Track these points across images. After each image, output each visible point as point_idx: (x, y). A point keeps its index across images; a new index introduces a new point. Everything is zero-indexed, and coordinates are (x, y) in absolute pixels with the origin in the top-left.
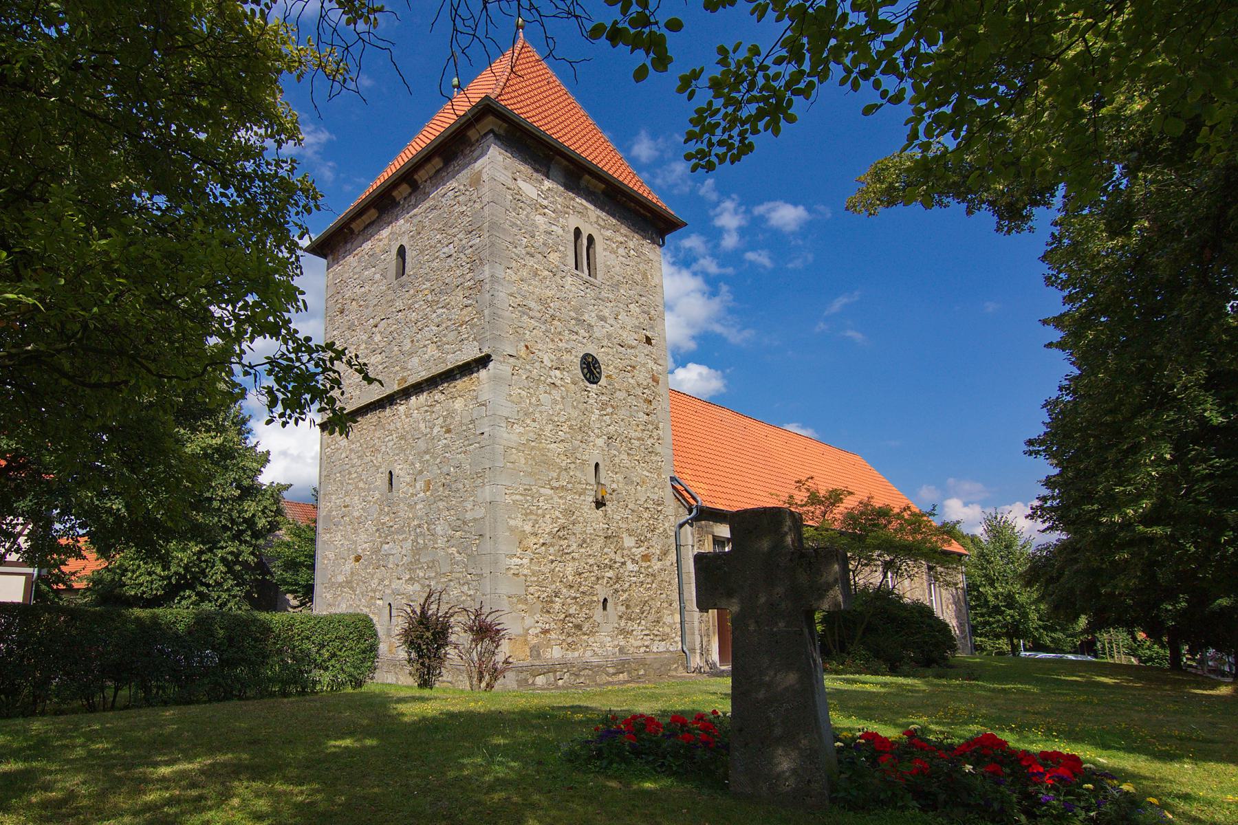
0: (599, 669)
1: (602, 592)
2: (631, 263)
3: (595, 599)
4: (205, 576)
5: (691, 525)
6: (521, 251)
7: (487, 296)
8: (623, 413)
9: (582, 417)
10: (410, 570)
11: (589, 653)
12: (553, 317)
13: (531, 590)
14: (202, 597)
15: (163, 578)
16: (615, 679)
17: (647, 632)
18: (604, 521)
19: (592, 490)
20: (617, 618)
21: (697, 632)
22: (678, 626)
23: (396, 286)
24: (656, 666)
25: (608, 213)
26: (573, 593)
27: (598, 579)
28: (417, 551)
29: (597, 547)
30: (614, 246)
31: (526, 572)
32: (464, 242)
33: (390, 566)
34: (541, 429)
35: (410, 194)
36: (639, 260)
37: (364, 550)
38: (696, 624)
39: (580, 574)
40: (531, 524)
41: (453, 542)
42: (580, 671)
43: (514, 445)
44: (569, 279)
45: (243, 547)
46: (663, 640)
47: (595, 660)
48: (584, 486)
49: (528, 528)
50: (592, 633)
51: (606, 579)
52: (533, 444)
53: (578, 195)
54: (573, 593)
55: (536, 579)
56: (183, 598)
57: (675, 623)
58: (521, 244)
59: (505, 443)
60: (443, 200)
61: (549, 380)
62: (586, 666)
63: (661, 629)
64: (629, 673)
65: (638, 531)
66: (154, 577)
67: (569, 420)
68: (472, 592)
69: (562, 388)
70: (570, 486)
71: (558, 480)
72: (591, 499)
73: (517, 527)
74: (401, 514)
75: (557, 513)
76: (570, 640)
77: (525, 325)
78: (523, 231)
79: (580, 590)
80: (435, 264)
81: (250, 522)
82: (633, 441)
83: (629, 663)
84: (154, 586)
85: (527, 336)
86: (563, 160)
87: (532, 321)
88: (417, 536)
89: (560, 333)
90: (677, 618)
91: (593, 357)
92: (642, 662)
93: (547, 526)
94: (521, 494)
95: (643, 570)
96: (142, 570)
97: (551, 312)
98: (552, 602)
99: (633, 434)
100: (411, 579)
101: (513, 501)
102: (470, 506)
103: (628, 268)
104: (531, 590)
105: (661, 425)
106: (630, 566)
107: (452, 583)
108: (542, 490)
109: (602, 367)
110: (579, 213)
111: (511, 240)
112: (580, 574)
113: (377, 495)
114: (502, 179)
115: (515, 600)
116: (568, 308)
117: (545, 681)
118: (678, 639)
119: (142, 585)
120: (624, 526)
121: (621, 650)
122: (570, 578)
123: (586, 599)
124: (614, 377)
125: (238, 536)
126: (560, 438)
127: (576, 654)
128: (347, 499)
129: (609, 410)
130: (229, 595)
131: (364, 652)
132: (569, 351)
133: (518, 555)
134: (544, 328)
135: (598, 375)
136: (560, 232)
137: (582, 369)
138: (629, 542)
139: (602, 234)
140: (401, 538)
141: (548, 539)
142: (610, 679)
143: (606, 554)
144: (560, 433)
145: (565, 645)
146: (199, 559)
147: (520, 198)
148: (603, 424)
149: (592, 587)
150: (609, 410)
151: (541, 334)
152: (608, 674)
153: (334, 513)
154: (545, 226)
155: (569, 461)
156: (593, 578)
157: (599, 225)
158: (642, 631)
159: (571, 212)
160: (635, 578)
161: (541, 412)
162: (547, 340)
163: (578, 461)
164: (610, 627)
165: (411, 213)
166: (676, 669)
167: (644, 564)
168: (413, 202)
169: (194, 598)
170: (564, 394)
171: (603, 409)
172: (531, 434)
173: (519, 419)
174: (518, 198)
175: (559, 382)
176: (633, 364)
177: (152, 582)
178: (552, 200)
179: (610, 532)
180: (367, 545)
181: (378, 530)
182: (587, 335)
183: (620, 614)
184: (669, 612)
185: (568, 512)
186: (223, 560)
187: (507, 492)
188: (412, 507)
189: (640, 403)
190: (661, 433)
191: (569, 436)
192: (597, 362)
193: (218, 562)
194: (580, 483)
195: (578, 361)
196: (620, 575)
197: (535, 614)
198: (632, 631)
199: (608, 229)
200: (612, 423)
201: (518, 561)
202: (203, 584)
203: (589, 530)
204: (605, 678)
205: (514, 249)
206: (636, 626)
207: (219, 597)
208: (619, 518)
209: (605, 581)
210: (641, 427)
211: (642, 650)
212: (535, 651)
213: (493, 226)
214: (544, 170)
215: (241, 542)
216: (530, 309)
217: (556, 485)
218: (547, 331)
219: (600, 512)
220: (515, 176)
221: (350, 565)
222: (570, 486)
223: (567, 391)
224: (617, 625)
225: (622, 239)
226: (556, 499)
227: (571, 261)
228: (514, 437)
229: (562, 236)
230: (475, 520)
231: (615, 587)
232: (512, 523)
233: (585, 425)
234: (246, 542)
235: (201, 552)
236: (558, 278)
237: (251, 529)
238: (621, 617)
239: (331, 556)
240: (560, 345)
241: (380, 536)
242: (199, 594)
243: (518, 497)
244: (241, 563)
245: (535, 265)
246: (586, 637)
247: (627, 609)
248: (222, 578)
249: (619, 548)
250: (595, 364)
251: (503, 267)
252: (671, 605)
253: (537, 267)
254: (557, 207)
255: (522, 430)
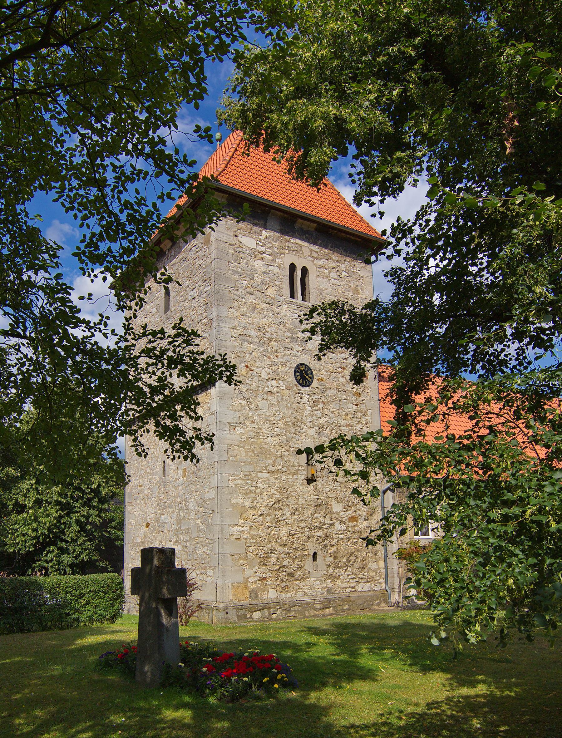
0: (309, 605)
1: (311, 548)
2: (343, 283)
3: (306, 553)
4: (65, 535)
5: (393, 491)
6: (242, 292)
7: (214, 331)
8: (333, 406)
9: (296, 415)
10: (176, 535)
11: (300, 594)
12: (270, 340)
13: (251, 549)
14: (63, 551)
15: (33, 538)
16: (322, 612)
17: (353, 576)
18: (315, 494)
19: (304, 470)
20: (325, 567)
21: (396, 575)
22: (383, 570)
23: (165, 319)
24: (360, 602)
25: (320, 246)
26: (286, 550)
27: (309, 538)
28: (180, 521)
29: (307, 513)
30: (326, 271)
31: (246, 536)
32: (201, 288)
33: (165, 531)
34: (259, 428)
35: (171, 247)
36: (350, 279)
37: (151, 519)
38: (395, 569)
39: (293, 535)
40: (250, 500)
41: (198, 515)
42: (291, 607)
43: (236, 443)
44: (285, 307)
45: (92, 511)
46: (368, 582)
47: (305, 598)
48: (297, 468)
49: (248, 504)
50: (302, 579)
51: (316, 537)
52: (252, 440)
53: (293, 236)
54: (286, 550)
55: (254, 541)
56: (49, 552)
57: (379, 569)
58: (242, 287)
59: (228, 442)
60: (190, 253)
61: (267, 389)
62: (296, 604)
63: (366, 574)
64: (335, 608)
65: (346, 499)
66: (27, 537)
67: (284, 418)
68: (209, 552)
69: (278, 394)
70: (284, 469)
71: (273, 465)
72: (303, 477)
73: (238, 504)
74: (170, 493)
75: (273, 491)
76: (283, 584)
77: (245, 350)
78: (244, 276)
79: (293, 547)
80: (186, 304)
81: (97, 492)
82: (342, 428)
83: (334, 600)
84: (27, 544)
85: (247, 358)
86: (277, 212)
87: (252, 346)
88: (179, 510)
89: (276, 351)
90: (382, 564)
91: (306, 365)
92: (347, 600)
93: (264, 501)
94: (242, 479)
95: (350, 529)
96: (19, 533)
97: (268, 335)
98: (268, 557)
99: (342, 423)
100: (176, 541)
101: (236, 485)
102: (207, 490)
103: (340, 288)
104: (251, 549)
105: (369, 412)
106: (338, 526)
107: (198, 545)
108: (260, 475)
109: (314, 372)
110: (293, 251)
111: (233, 286)
112: (293, 535)
113: (157, 479)
114: (225, 238)
115: (237, 557)
116: (284, 329)
117: (260, 615)
118: (382, 580)
119: (18, 544)
120: (333, 495)
121: (329, 591)
122: (284, 539)
123: (298, 553)
124: (325, 378)
125: (87, 503)
126: (276, 433)
127: (289, 595)
128: (141, 480)
129: (321, 406)
130: (82, 549)
131: (111, 600)
132: (283, 364)
133: (240, 524)
134: (261, 349)
135: (310, 380)
136: (276, 270)
137: (296, 377)
138: (337, 508)
139: (315, 264)
140: (171, 511)
141: (264, 510)
142: (317, 613)
143: (316, 518)
144: (276, 429)
145: (279, 588)
146: (59, 522)
147: (241, 250)
148: (314, 417)
149: (303, 545)
150: (321, 406)
151: (260, 354)
152: (315, 609)
153: (134, 491)
154: (262, 268)
155: (283, 450)
156: (304, 538)
157: (312, 257)
158: (348, 575)
159: (287, 252)
160: (342, 536)
161: (259, 415)
162: (265, 358)
163: (291, 449)
164: (319, 574)
165: (172, 262)
166: (378, 604)
167: (351, 524)
168: (173, 254)
169: (56, 552)
170: (279, 398)
171: (315, 406)
172: (251, 433)
173: (240, 423)
174: (239, 250)
175: (275, 389)
176: (344, 365)
177: (25, 541)
178: (269, 245)
179: (320, 501)
180: (152, 515)
181: (158, 504)
182: (300, 349)
183: (328, 563)
184: (374, 560)
185: (283, 489)
186: (77, 522)
187: (230, 478)
188: (176, 488)
189: (349, 396)
190: (369, 418)
191: (284, 431)
192: (309, 369)
193: (73, 524)
194: (293, 466)
195: (292, 371)
196: (328, 534)
197: (254, 567)
198: (340, 576)
199: (321, 259)
200: (322, 416)
201: (241, 529)
202: (62, 541)
203: (301, 501)
204: (313, 612)
205: (236, 292)
206: (343, 572)
207: (74, 550)
208: (328, 489)
209: (315, 539)
210: (350, 416)
211: (348, 590)
212: (254, 594)
213: (219, 276)
214: (262, 222)
215: (90, 507)
216: (250, 337)
217: (271, 469)
218: (264, 351)
219: (311, 487)
220: (236, 233)
221: (143, 530)
222: (284, 469)
223: (282, 396)
224: (325, 572)
225: (334, 265)
226: (272, 480)
227: (287, 292)
228: (236, 437)
229: (278, 273)
230: (210, 499)
231: (325, 543)
232: (234, 501)
233: (298, 420)
234: (94, 507)
235: (61, 517)
236: (274, 307)
237: (98, 497)
238: (329, 566)
239: (133, 523)
240: (276, 360)
241: (159, 509)
242: (60, 549)
243: (239, 482)
244: (90, 523)
245: (254, 301)
246: (297, 582)
247: (335, 559)
248: (76, 536)
249: (328, 513)
250: (308, 370)
251: (226, 307)
252: (376, 554)
253: (256, 302)
254: (274, 251)
255: (242, 430)
